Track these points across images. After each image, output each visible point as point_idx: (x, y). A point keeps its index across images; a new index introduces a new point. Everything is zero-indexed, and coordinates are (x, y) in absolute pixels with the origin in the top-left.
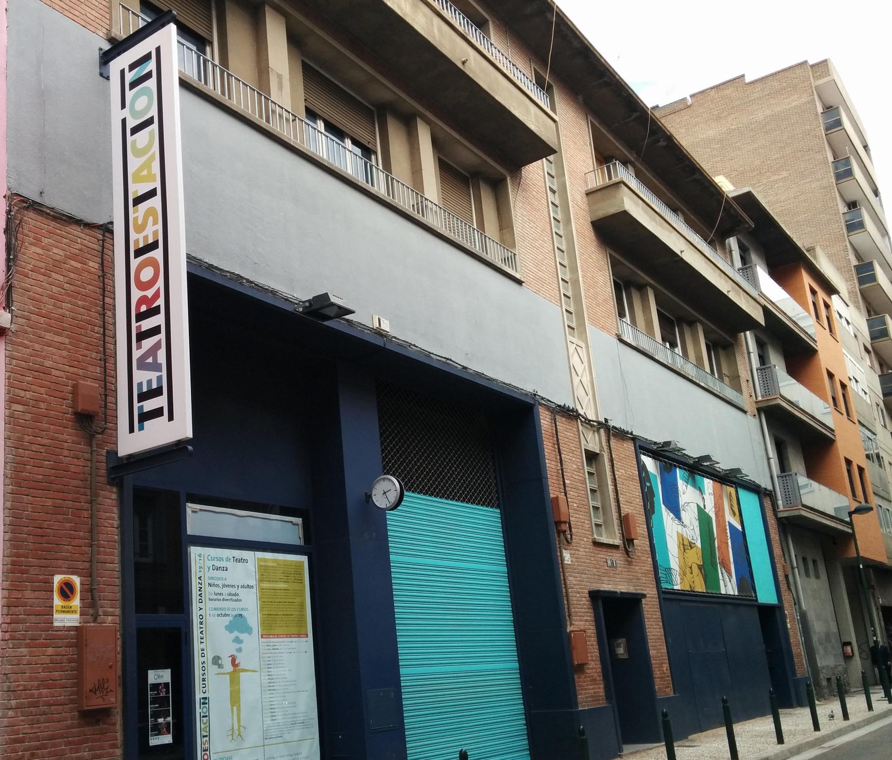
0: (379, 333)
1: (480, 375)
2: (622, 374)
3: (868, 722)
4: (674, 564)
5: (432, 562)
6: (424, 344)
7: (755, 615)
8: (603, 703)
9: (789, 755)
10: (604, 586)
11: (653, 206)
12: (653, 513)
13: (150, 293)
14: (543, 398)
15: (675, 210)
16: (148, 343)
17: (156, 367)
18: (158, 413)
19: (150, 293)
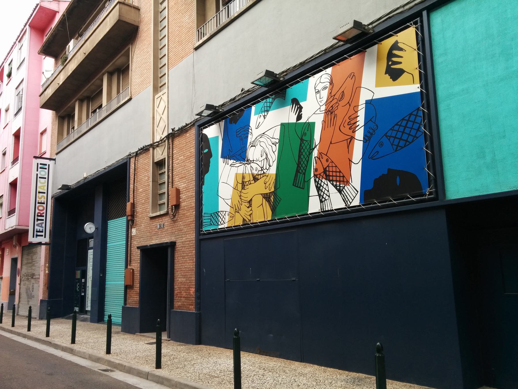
0: (86, 178)
1: (109, 167)
2: (194, 77)
3: (64, 349)
4: (224, 206)
5: (117, 243)
6: (109, 164)
7: (440, 220)
8: (137, 306)
9: (87, 357)
10: (153, 241)
11: (94, 29)
12: (207, 171)
13: (42, 212)
14: (223, 105)
15: (103, 7)
16: (39, 222)
17: (42, 227)
18: (42, 236)
19: (42, 212)
